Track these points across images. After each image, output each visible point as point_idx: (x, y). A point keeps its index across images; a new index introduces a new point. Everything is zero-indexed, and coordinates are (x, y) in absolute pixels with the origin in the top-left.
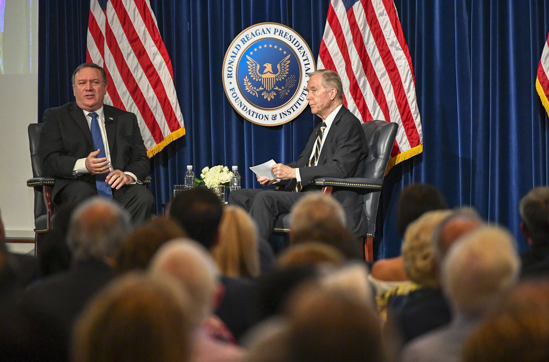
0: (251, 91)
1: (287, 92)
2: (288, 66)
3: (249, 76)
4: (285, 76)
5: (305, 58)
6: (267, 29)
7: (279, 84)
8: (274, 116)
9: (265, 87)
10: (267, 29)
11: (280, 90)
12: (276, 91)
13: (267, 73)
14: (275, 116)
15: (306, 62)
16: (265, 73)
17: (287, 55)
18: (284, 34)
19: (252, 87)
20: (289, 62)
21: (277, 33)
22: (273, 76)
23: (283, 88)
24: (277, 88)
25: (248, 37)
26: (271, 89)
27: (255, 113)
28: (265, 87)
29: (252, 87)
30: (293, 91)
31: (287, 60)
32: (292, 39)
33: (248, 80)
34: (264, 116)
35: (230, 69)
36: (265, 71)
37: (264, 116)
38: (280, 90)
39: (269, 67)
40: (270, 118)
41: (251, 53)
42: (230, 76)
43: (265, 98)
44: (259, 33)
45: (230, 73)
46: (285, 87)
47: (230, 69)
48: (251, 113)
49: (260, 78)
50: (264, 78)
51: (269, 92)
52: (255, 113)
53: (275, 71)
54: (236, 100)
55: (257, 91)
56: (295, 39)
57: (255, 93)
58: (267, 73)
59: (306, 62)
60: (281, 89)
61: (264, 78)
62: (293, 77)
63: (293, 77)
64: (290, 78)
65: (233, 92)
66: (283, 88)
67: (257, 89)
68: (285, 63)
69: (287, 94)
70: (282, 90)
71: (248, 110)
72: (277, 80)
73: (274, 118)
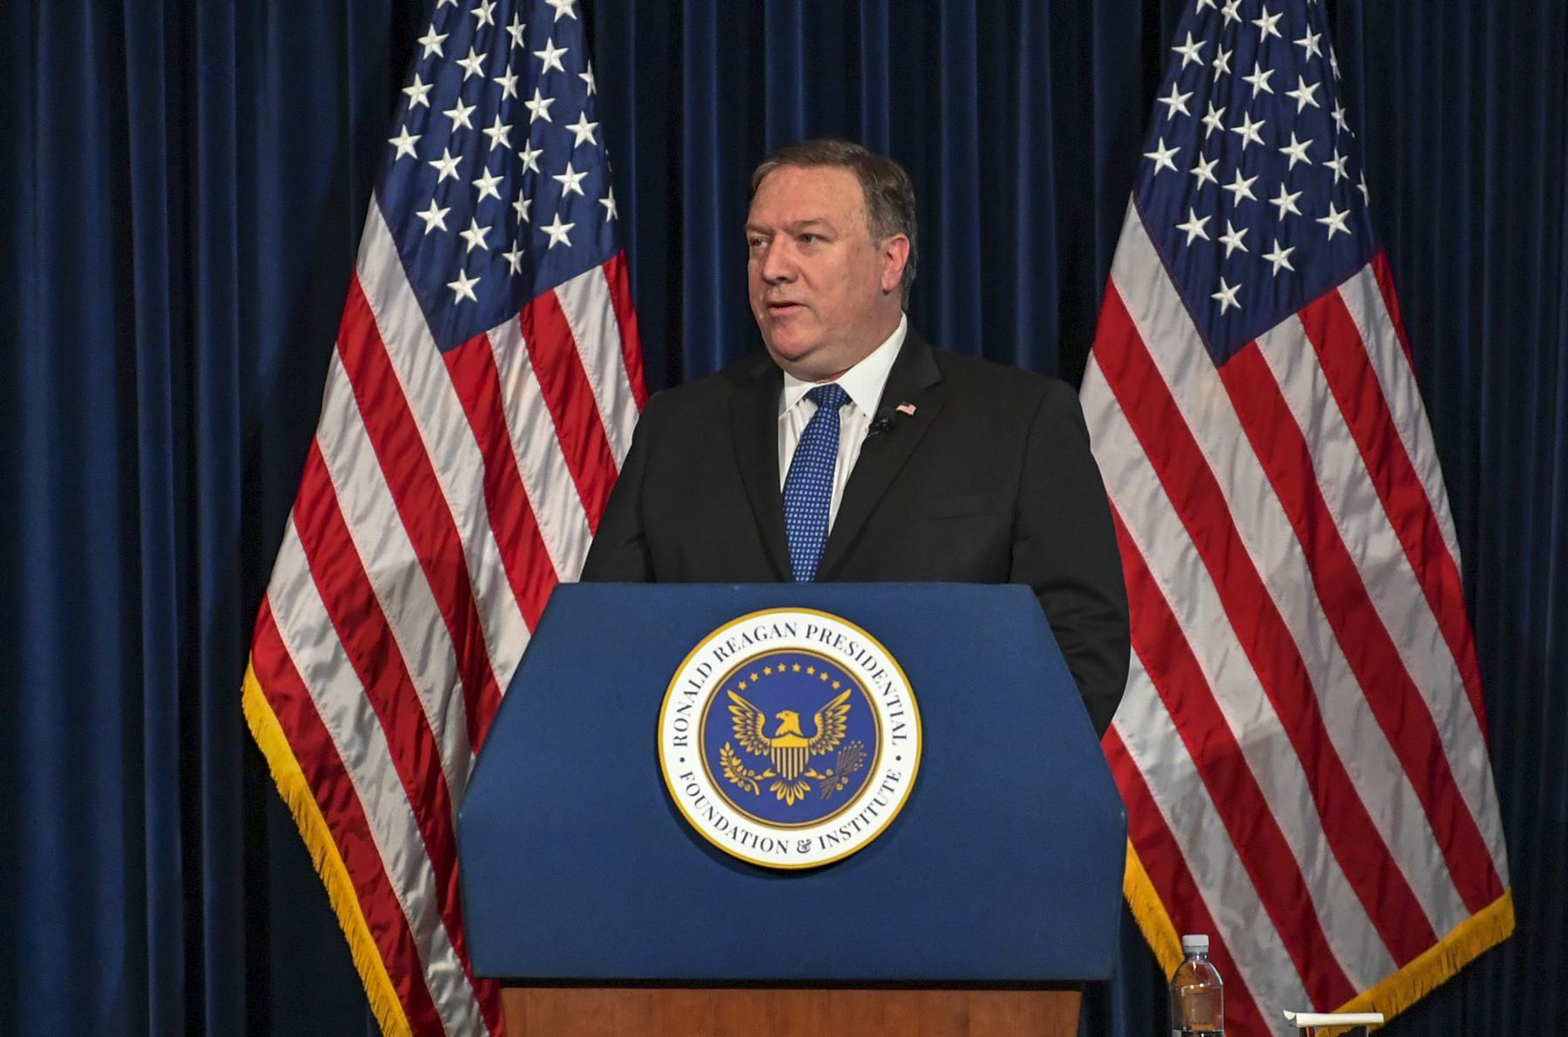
0: (740, 779)
1: (840, 782)
2: (844, 719)
3: (735, 744)
4: (837, 743)
5: (890, 697)
6: (787, 626)
7: (816, 762)
8: (803, 842)
9: (779, 770)
10: (787, 626)
11: (821, 777)
12: (810, 781)
13: (785, 734)
14: (806, 843)
15: (895, 709)
16: (780, 736)
17: (840, 691)
18: (833, 639)
19: (742, 771)
20: (846, 708)
21: (815, 637)
22: (804, 743)
23: (829, 772)
24: (812, 773)
25: (734, 645)
26: (796, 775)
27: (751, 835)
28: (779, 770)
29: (742, 771)
30: (858, 780)
31: (843, 704)
32: (856, 654)
33: (731, 753)
34: (775, 843)
35: (681, 725)
36: (781, 730)
37: (775, 843)
38: (821, 777)
39: (790, 720)
40: (792, 848)
41: (742, 686)
42: (681, 743)
43: (779, 797)
44: (766, 636)
45: (681, 735)
46: (834, 771)
47: (681, 725)
48: (740, 836)
49: (765, 747)
50: (776, 749)
51: (790, 784)
52: (751, 835)
53: (807, 729)
54: (697, 802)
55: (757, 782)
56: (863, 651)
57: (753, 787)
58: (785, 734)
59: (895, 709)
60: (824, 774)
61: (776, 749)
62: (859, 746)
63: (859, 746)
64: (850, 747)
65: (690, 782)
66: (829, 772)
67: (756, 775)
68: (835, 711)
69: (840, 788)
70: (828, 777)
71: (731, 827)
72: (814, 753)
73: (805, 847)
